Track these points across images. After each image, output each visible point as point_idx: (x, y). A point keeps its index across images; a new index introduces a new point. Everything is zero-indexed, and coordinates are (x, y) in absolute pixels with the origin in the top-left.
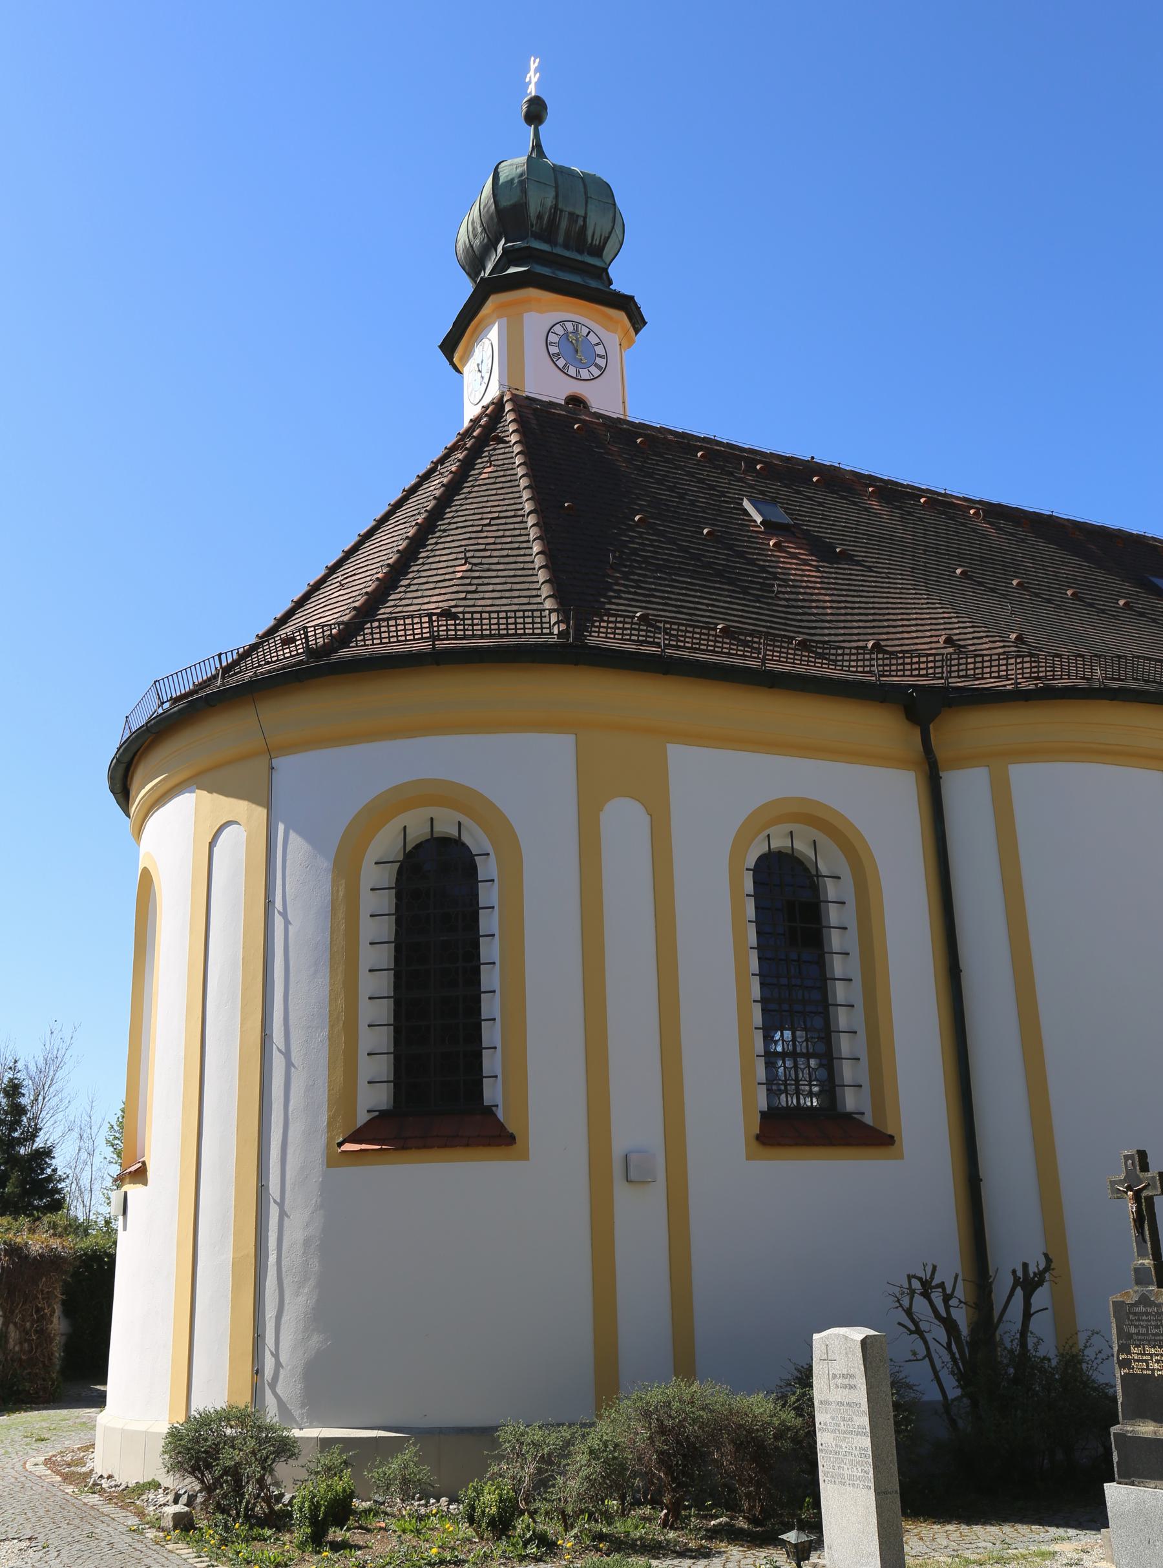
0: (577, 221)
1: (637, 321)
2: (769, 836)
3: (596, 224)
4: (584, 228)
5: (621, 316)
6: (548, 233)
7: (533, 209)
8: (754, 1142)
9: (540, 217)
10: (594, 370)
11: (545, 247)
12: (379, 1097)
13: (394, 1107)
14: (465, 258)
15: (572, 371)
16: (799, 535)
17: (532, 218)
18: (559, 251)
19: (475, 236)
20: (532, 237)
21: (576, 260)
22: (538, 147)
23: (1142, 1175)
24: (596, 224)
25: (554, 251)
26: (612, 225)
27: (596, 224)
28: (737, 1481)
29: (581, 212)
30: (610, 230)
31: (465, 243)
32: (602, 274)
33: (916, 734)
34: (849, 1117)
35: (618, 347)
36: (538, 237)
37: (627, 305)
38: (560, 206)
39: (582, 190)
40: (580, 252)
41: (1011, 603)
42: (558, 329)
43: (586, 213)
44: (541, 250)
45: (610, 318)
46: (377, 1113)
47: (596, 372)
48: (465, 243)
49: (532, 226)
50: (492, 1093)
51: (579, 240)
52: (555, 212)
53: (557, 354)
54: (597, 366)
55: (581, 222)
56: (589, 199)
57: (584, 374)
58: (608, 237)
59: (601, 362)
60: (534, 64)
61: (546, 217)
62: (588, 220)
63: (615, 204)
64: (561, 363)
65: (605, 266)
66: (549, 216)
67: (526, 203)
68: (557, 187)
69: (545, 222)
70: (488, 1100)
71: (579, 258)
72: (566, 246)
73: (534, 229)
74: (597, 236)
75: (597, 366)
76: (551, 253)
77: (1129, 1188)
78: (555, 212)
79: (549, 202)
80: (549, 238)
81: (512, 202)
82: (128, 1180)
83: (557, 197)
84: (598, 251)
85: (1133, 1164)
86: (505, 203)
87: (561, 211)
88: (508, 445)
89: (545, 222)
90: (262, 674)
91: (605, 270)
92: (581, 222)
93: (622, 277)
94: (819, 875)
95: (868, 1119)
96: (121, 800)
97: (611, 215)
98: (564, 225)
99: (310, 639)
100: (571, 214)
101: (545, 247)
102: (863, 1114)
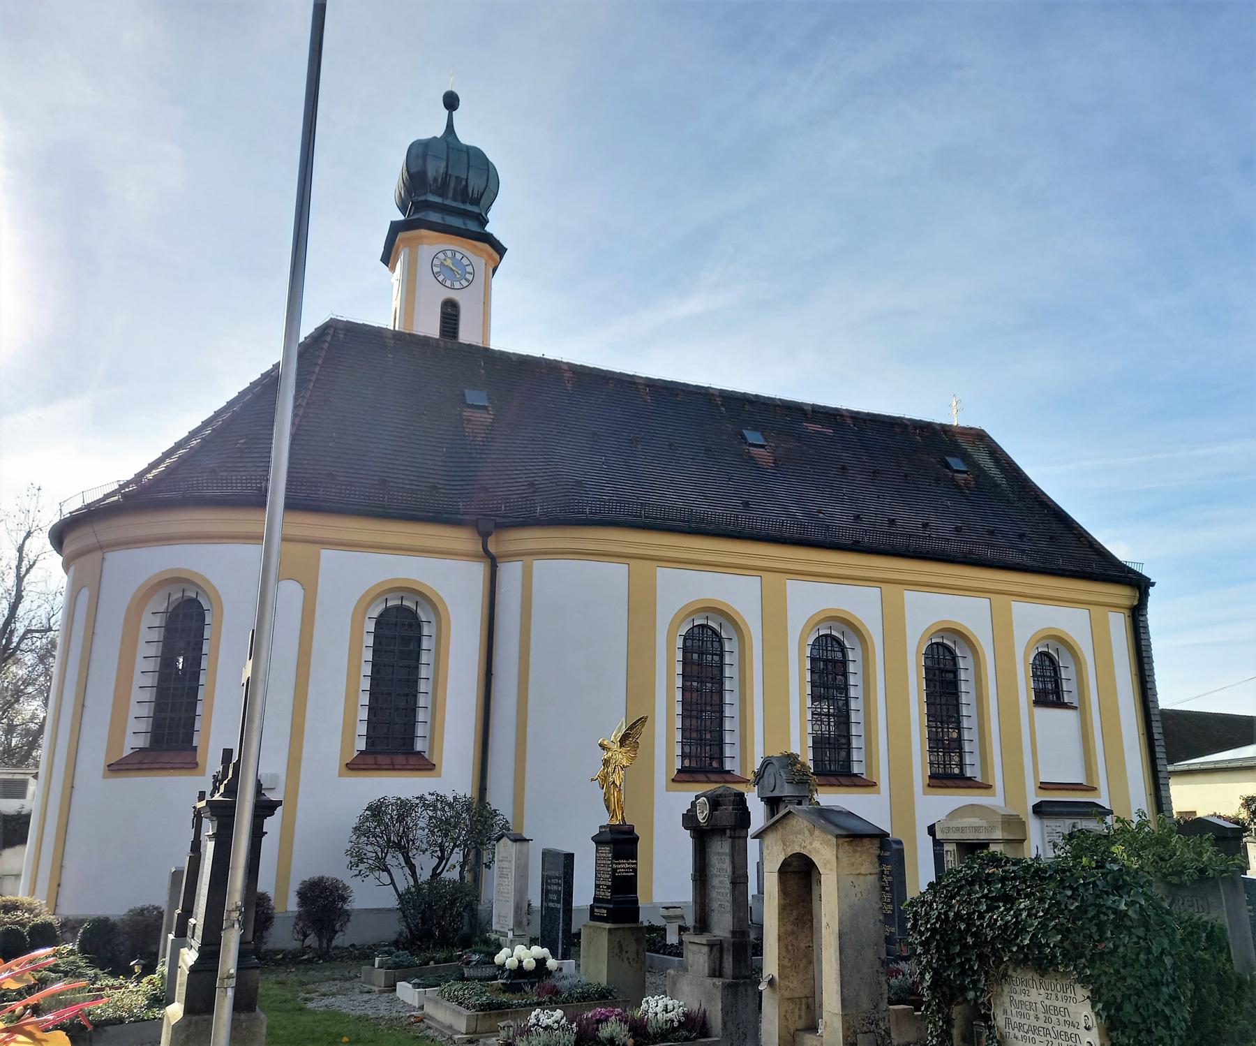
0: (461, 182)
2: (387, 599)
3: (475, 184)
4: (466, 186)
5: (487, 247)
6: (442, 190)
7: (431, 174)
9: (435, 180)
11: (438, 200)
12: (361, 745)
15: (448, 283)
18: (449, 202)
20: (430, 192)
29: (464, 176)
30: (484, 188)
32: (484, 222)
38: (449, 172)
39: (466, 161)
40: (464, 202)
41: (604, 456)
42: (441, 256)
43: (467, 177)
44: (435, 202)
47: (465, 283)
50: (419, 746)
51: (463, 195)
52: (446, 177)
53: (437, 273)
55: (464, 183)
56: (470, 168)
57: (457, 285)
59: (470, 277)
60: (181, 660)
61: (440, 180)
62: (469, 181)
64: (441, 278)
66: (442, 179)
71: (462, 206)
72: (454, 199)
73: (432, 187)
74: (476, 192)
78: (446, 177)
79: (442, 170)
80: (442, 190)
82: (401, 246)
83: (447, 166)
84: (476, 201)
87: (450, 176)
92: (464, 183)
98: (452, 185)
99: (1048, 674)
100: (457, 178)
101: (438, 200)
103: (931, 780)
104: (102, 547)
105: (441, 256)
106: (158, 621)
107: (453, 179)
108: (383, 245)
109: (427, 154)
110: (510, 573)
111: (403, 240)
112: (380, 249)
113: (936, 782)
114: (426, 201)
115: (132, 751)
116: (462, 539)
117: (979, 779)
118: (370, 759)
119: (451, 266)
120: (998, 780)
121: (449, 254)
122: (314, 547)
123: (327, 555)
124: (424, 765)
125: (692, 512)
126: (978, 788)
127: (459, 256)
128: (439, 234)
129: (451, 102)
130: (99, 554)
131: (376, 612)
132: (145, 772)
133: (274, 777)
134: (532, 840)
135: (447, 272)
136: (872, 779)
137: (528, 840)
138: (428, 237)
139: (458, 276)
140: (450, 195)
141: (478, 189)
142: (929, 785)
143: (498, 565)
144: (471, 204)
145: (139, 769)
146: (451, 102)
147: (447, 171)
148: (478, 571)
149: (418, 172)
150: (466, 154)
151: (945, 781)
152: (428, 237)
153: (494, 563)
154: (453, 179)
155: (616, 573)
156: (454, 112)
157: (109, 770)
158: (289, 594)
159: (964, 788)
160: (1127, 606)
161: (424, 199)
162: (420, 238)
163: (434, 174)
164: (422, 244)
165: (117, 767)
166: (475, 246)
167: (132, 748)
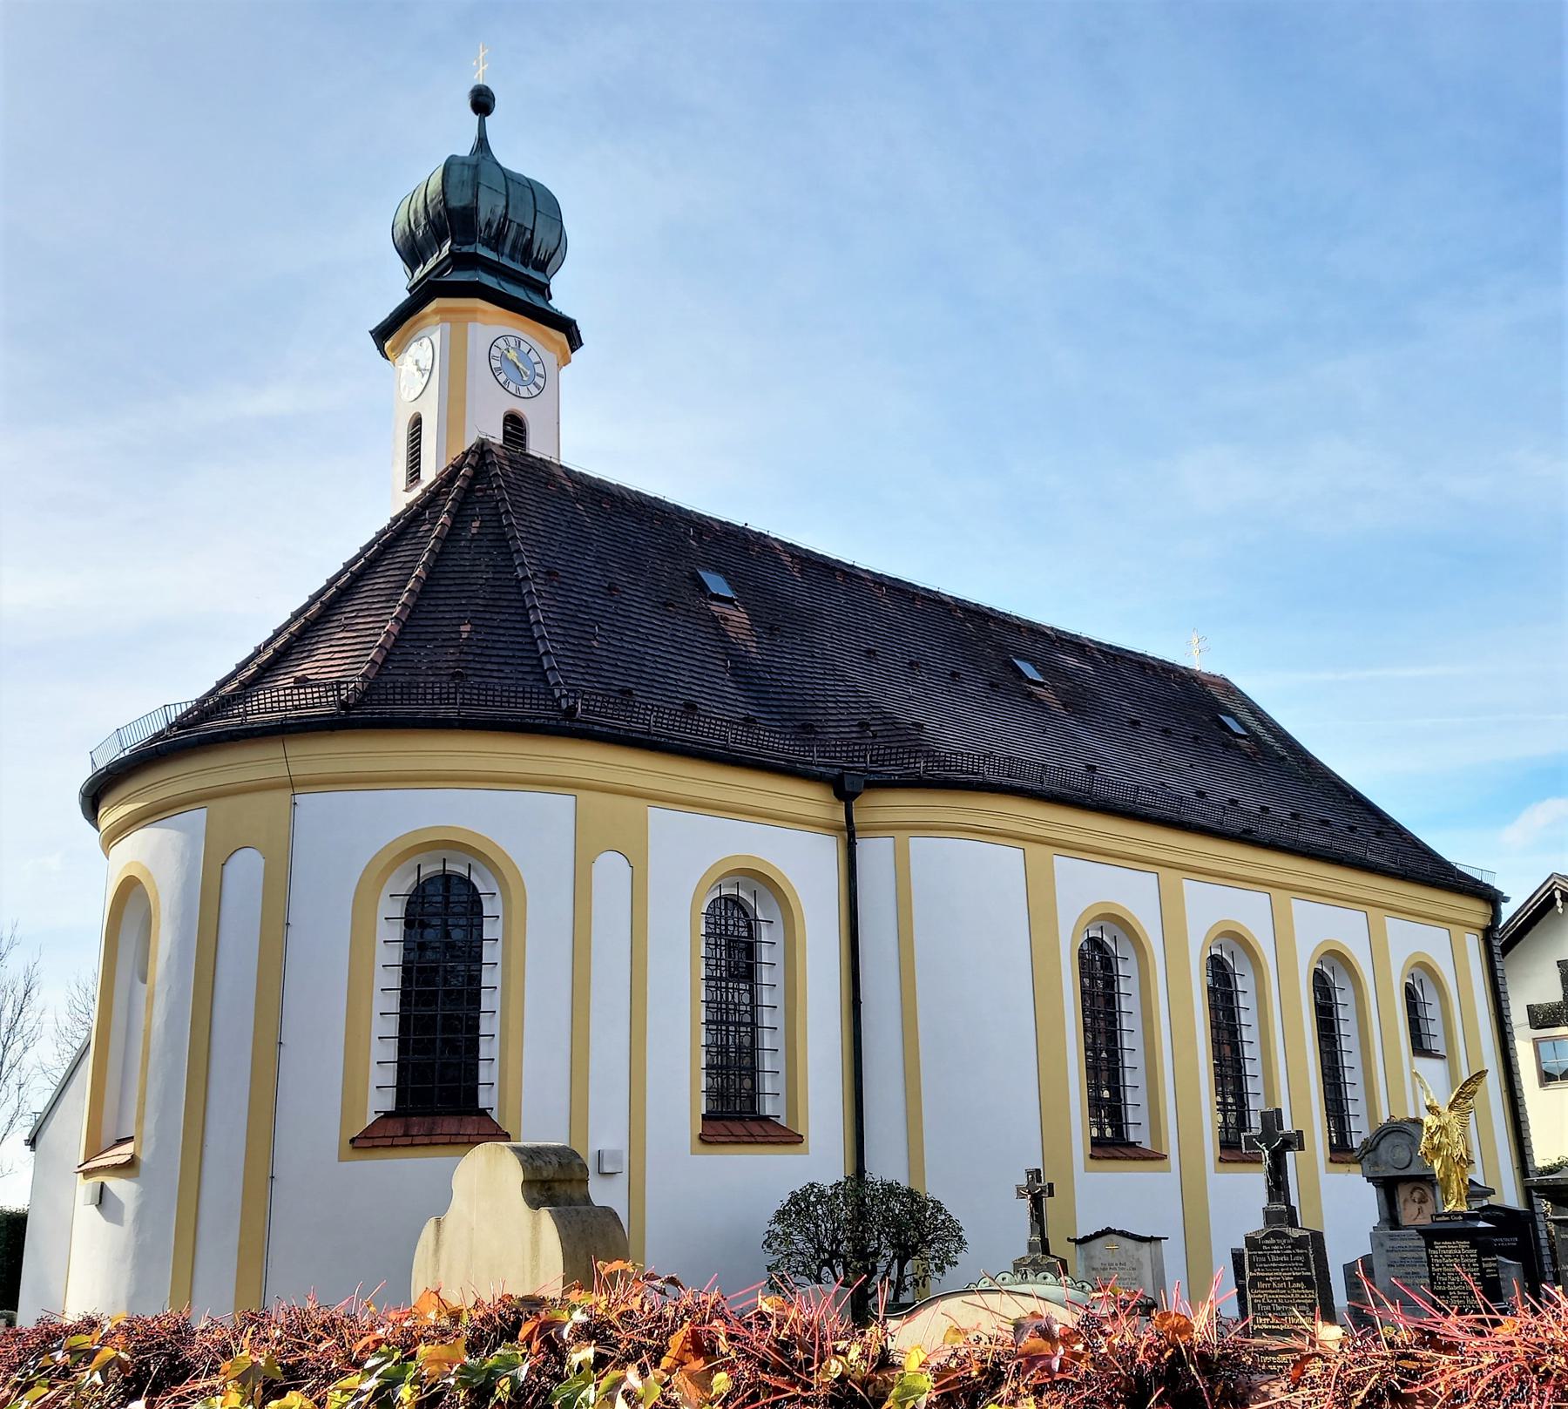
0: (524, 233)
1: (575, 341)
3: (543, 239)
4: (531, 241)
5: (561, 337)
7: (483, 216)
8: (696, 1140)
9: (489, 224)
10: (532, 387)
11: (492, 256)
12: (380, 1099)
13: (396, 1108)
14: (404, 245)
16: (741, 610)
17: (481, 224)
18: (505, 261)
19: (417, 227)
21: (523, 274)
22: (482, 143)
23: (1038, 1184)
24: (542, 239)
25: (501, 261)
26: (558, 242)
27: (542, 239)
28: (1373, 1403)
31: (404, 230)
32: (543, 290)
33: (842, 807)
34: (766, 1118)
35: (556, 366)
36: (486, 243)
37: (568, 329)
38: (509, 216)
45: (552, 339)
46: (382, 1114)
47: (535, 391)
48: (404, 230)
49: (481, 233)
50: (485, 1099)
51: (525, 251)
52: (504, 225)
53: (499, 369)
54: (536, 385)
55: (528, 235)
56: (538, 213)
58: (554, 254)
59: (540, 381)
61: (495, 226)
62: (535, 234)
63: (561, 222)
65: (546, 281)
67: (476, 208)
68: (507, 196)
69: (493, 230)
70: (483, 1103)
71: (524, 271)
74: (542, 251)
75: (536, 385)
76: (498, 263)
77: (1029, 1193)
79: (500, 211)
80: (496, 242)
81: (462, 204)
83: (507, 207)
84: (542, 266)
85: (1033, 1177)
86: (455, 203)
87: (511, 221)
88: (1419, 1326)
89: (493, 230)
90: (291, 718)
91: (548, 286)
92: (528, 235)
93: (564, 295)
94: (756, 920)
95: (782, 1122)
96: (88, 806)
97: (558, 232)
98: (512, 235)
101: (492, 256)
102: (778, 1117)
103: (1095, 1149)
104: (293, 785)
105: (501, 343)
106: (398, 909)
107: (514, 226)
108: (392, 311)
109: (479, 183)
110: (874, 853)
111: (437, 311)
112: (381, 313)
113: (1099, 1152)
114: (475, 254)
115: (375, 1117)
116: (811, 800)
117: (1146, 1145)
118: (395, 1127)
119: (516, 360)
120: (1172, 1149)
121: (512, 341)
122: (642, 803)
123: (657, 816)
124: (788, 1138)
125: (1093, 779)
126: (1145, 1159)
127: (524, 347)
128: (502, 309)
129: (482, 102)
130: (284, 796)
131: (407, 884)
132: (421, 1150)
133: (615, 1155)
134: (1167, 1238)
135: (509, 371)
136: (1161, 1150)
137: (1160, 1239)
138: (484, 312)
139: (525, 378)
140: (507, 250)
141: (547, 246)
142: (1092, 1157)
143: (857, 841)
144: (536, 268)
145: (392, 1146)
146: (482, 102)
147: (506, 214)
148: (828, 850)
149: (464, 208)
150: (530, 191)
151: (1111, 1150)
152: (484, 312)
153: (850, 837)
154: (514, 226)
155: (1010, 858)
156: (486, 118)
157: (354, 1148)
158: (610, 871)
159: (1135, 1159)
160: (1482, 927)
161: (472, 251)
162: (473, 311)
163: (489, 216)
164: (475, 320)
165: (367, 1142)
166: (545, 334)
167: (376, 1112)
